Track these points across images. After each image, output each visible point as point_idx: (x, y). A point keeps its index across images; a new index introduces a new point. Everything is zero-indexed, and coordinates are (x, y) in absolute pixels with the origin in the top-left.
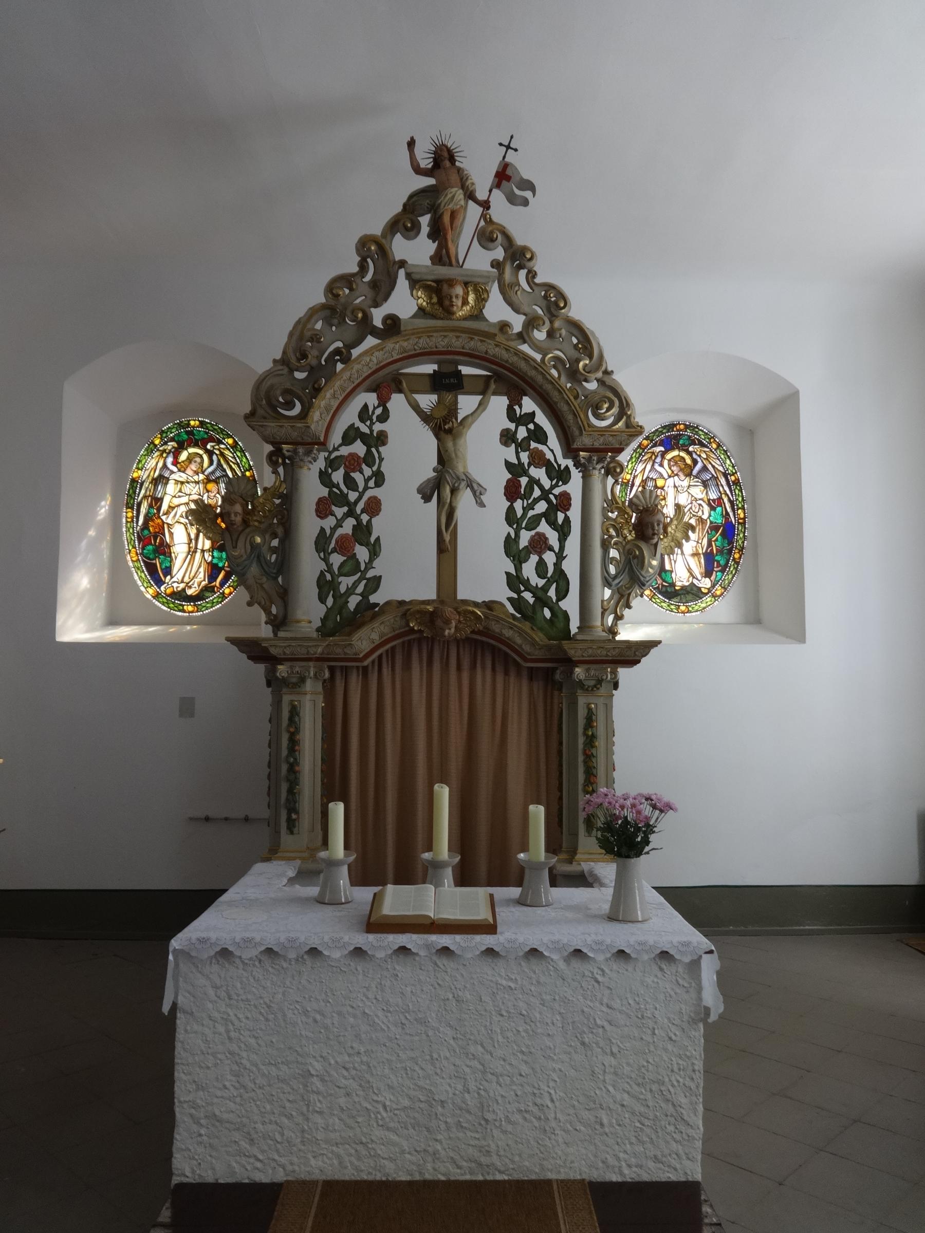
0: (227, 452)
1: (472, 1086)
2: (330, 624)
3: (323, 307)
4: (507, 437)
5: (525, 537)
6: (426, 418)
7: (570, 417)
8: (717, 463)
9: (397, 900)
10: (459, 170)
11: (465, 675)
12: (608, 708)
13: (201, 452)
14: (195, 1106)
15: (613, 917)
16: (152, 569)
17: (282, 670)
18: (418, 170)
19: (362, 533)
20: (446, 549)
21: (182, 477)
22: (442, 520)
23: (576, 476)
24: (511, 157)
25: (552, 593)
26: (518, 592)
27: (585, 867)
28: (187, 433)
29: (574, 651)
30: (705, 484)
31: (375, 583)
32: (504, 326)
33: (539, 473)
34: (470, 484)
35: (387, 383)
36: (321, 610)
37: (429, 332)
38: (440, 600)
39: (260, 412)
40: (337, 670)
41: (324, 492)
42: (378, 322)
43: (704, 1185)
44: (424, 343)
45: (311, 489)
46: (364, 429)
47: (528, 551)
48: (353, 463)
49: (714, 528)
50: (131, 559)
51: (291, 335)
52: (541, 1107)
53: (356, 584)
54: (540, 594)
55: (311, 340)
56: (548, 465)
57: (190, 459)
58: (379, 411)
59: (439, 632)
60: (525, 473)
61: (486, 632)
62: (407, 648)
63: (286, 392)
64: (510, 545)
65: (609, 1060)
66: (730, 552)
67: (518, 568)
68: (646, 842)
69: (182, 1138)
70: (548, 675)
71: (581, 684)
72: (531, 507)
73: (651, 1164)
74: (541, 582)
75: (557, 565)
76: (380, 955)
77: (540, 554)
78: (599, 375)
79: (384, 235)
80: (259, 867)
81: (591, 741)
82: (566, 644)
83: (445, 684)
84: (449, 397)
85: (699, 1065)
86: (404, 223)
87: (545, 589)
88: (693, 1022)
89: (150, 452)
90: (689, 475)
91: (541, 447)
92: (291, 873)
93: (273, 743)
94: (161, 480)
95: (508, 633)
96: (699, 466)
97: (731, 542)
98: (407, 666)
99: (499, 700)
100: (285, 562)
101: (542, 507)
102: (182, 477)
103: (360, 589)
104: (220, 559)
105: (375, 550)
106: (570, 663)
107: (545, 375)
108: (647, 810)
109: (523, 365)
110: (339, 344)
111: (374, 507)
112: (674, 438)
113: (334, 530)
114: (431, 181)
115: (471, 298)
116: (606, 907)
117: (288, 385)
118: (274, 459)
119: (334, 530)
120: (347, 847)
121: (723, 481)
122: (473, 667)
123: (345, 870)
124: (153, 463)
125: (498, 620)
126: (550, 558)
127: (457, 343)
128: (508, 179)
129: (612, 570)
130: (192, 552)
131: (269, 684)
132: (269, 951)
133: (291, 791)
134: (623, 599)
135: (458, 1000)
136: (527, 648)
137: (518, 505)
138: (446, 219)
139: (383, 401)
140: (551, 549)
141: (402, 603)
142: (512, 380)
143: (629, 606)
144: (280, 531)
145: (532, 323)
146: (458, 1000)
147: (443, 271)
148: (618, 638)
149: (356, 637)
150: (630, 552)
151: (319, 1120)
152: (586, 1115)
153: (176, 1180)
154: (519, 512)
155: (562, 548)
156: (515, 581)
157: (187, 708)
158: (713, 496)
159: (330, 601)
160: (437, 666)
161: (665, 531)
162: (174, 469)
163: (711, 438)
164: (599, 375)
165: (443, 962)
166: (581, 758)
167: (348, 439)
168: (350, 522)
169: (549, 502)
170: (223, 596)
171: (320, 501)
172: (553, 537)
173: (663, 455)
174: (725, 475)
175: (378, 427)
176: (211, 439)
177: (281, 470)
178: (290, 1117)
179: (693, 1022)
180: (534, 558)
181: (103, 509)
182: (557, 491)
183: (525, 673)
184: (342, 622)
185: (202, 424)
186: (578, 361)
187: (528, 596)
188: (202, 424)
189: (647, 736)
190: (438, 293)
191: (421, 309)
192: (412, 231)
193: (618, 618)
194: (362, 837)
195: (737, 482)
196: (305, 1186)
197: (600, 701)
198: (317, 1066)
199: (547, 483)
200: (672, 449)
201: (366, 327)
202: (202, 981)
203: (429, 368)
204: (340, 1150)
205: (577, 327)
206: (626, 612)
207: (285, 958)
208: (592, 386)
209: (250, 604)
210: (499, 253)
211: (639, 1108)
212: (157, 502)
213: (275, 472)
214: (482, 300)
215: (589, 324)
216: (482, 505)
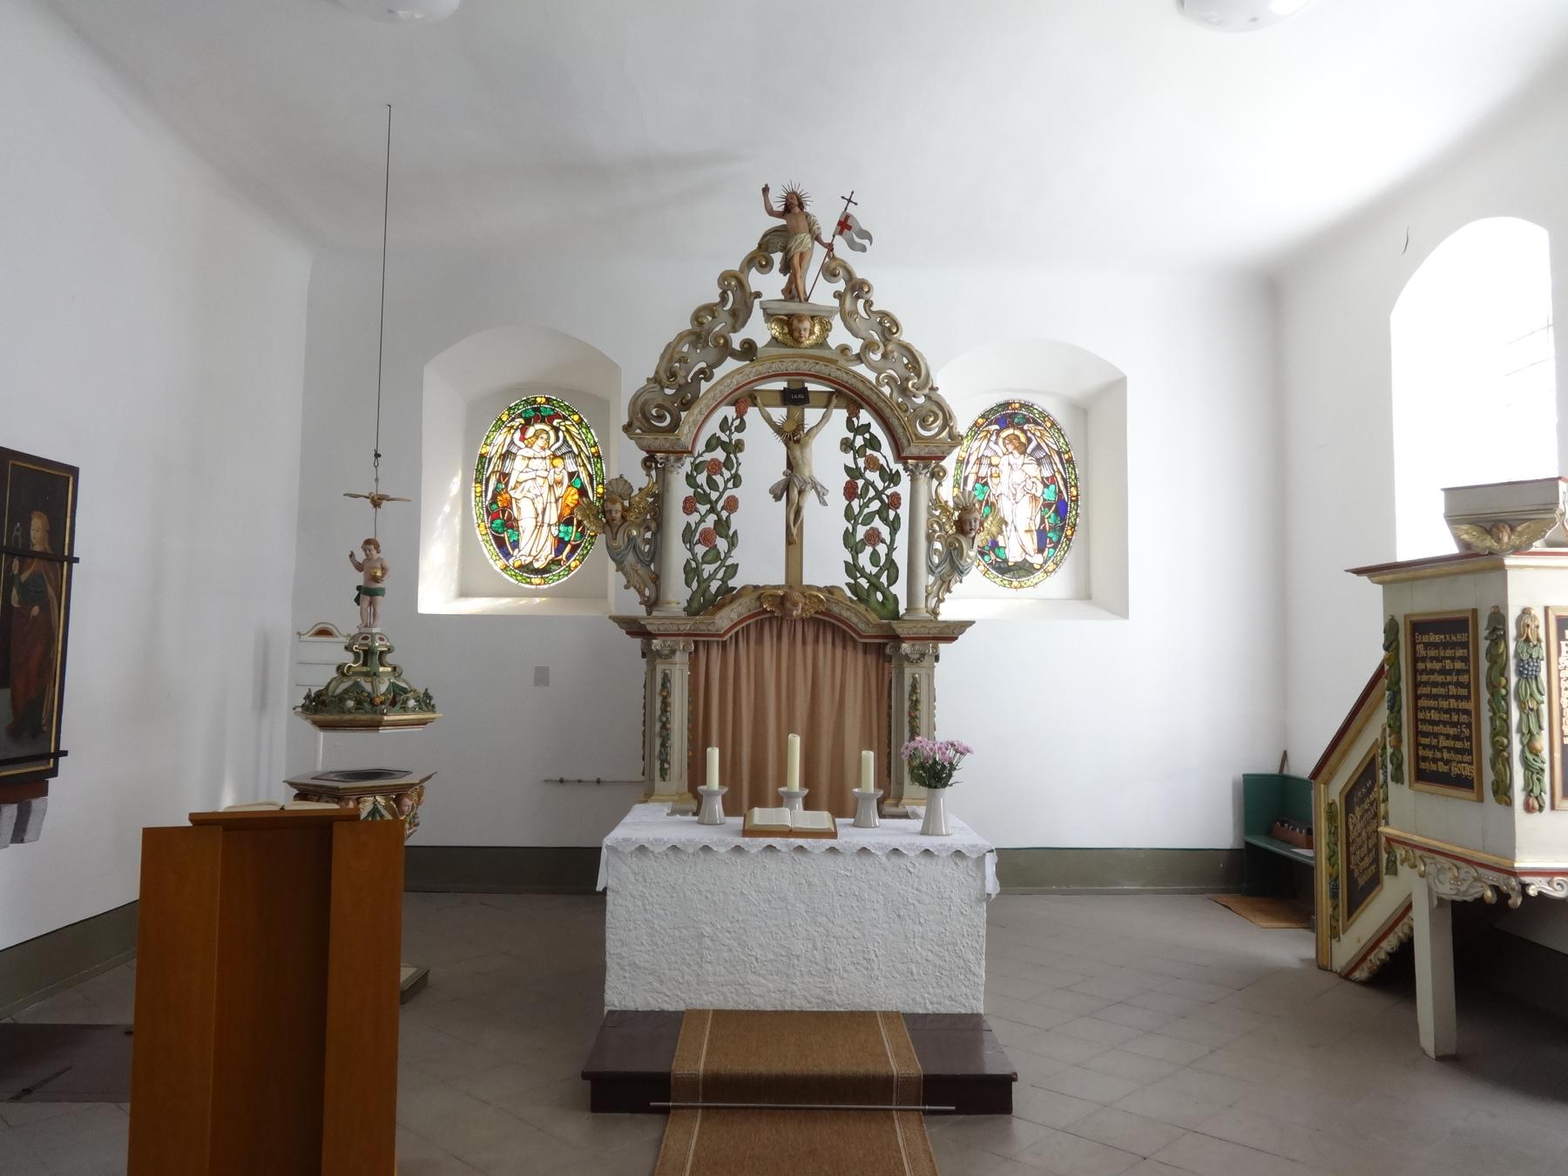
0: (572, 429)
1: (819, 945)
2: (695, 605)
3: (690, 333)
4: (847, 445)
5: (861, 532)
6: (779, 430)
7: (900, 430)
8: (1050, 441)
9: (760, 816)
10: (807, 215)
11: (809, 649)
12: (930, 677)
13: (547, 428)
14: (622, 958)
15: (923, 833)
16: (500, 543)
17: (656, 644)
18: (771, 213)
19: (722, 527)
20: (793, 541)
21: (528, 452)
22: (787, 518)
23: (905, 478)
24: (852, 209)
25: (884, 579)
26: (855, 579)
27: (909, 809)
28: (535, 410)
29: (901, 629)
30: (1039, 462)
31: (733, 569)
32: (844, 349)
33: (873, 476)
34: (815, 486)
35: (744, 398)
36: (688, 593)
37: (781, 358)
38: (789, 585)
39: (636, 423)
40: (701, 643)
41: (690, 492)
42: (736, 345)
43: (991, 1023)
44: (776, 367)
45: (680, 490)
46: (724, 438)
47: (864, 543)
48: (715, 467)
49: (1048, 505)
50: (481, 533)
51: (662, 357)
52: (868, 960)
53: (716, 572)
54: (874, 580)
55: (679, 361)
56: (881, 469)
57: (536, 435)
58: (737, 422)
59: (782, 612)
60: (861, 476)
61: (828, 613)
62: (760, 626)
63: (659, 406)
64: (848, 537)
65: (918, 928)
66: (1062, 529)
67: (855, 558)
68: (950, 776)
69: (611, 980)
70: (880, 649)
71: (907, 657)
72: (867, 505)
73: (947, 1002)
74: (875, 570)
75: (888, 555)
76: (753, 851)
77: (874, 546)
78: (926, 391)
79: (741, 270)
80: (637, 806)
81: (915, 704)
82: (895, 624)
83: (792, 657)
84: (796, 411)
85: (983, 932)
86: (759, 260)
87: (878, 576)
88: (979, 901)
89: (498, 428)
90: (1023, 453)
91: (875, 454)
92: (668, 810)
93: (647, 706)
94: (507, 455)
95: (846, 614)
96: (1034, 444)
97: (1063, 519)
98: (760, 641)
99: (838, 672)
100: (656, 553)
101: (875, 505)
102: (528, 452)
103: (720, 575)
104: (566, 533)
105: (733, 542)
106: (898, 639)
107: (879, 394)
108: (951, 753)
109: (860, 386)
110: (703, 365)
111: (732, 505)
112: (1007, 417)
113: (698, 524)
114: (782, 222)
115: (817, 329)
116: (920, 829)
117: (660, 401)
118: (648, 463)
119: (698, 524)
120: (722, 782)
121: (1056, 459)
122: (816, 641)
123: (719, 799)
124: (501, 439)
125: (838, 603)
126: (882, 549)
127: (804, 368)
128: (849, 228)
129: (936, 560)
130: (539, 526)
131: (644, 655)
132: (674, 847)
133: (663, 745)
134: (945, 584)
135: (810, 884)
136: (862, 626)
137: (856, 504)
138: (796, 261)
139: (741, 414)
140: (883, 541)
141: (756, 588)
142: (851, 397)
143: (949, 591)
144: (653, 525)
145: (869, 346)
146: (810, 884)
147: (793, 307)
148: (940, 618)
149: (718, 616)
150: (951, 545)
151: (708, 967)
152: (901, 966)
153: (606, 1009)
154: (856, 510)
155: (892, 541)
156: (852, 569)
157: (542, 676)
158: (1047, 473)
159: (695, 585)
160: (785, 640)
161: (982, 524)
162: (521, 445)
163: (1045, 415)
164: (926, 391)
165: (798, 857)
166: (907, 719)
167: (710, 447)
168: (712, 518)
169: (882, 501)
170: (569, 569)
171: (687, 500)
172: (885, 531)
173: (998, 433)
174: (1059, 453)
175: (736, 436)
176: (557, 416)
177: (653, 473)
178: (689, 966)
179: (979, 901)
180: (869, 550)
181: (455, 485)
182: (888, 492)
183: (860, 648)
184: (705, 603)
185: (548, 400)
186: (908, 380)
187: (863, 582)
188: (548, 400)
189: (961, 697)
190: (789, 325)
191: (774, 338)
192: (766, 266)
193: (940, 601)
194: (729, 774)
195: (1070, 461)
196: (701, 1013)
197: (923, 672)
198: (708, 930)
199: (880, 485)
200: (1007, 427)
201: (726, 350)
202: (625, 869)
203: (781, 385)
204: (725, 989)
205: (907, 349)
206: (947, 596)
207: (685, 852)
208: (920, 400)
209: (626, 587)
210: (841, 286)
211: (938, 962)
212: (505, 476)
213: (648, 475)
214: (826, 328)
215: (918, 346)
216: (824, 503)
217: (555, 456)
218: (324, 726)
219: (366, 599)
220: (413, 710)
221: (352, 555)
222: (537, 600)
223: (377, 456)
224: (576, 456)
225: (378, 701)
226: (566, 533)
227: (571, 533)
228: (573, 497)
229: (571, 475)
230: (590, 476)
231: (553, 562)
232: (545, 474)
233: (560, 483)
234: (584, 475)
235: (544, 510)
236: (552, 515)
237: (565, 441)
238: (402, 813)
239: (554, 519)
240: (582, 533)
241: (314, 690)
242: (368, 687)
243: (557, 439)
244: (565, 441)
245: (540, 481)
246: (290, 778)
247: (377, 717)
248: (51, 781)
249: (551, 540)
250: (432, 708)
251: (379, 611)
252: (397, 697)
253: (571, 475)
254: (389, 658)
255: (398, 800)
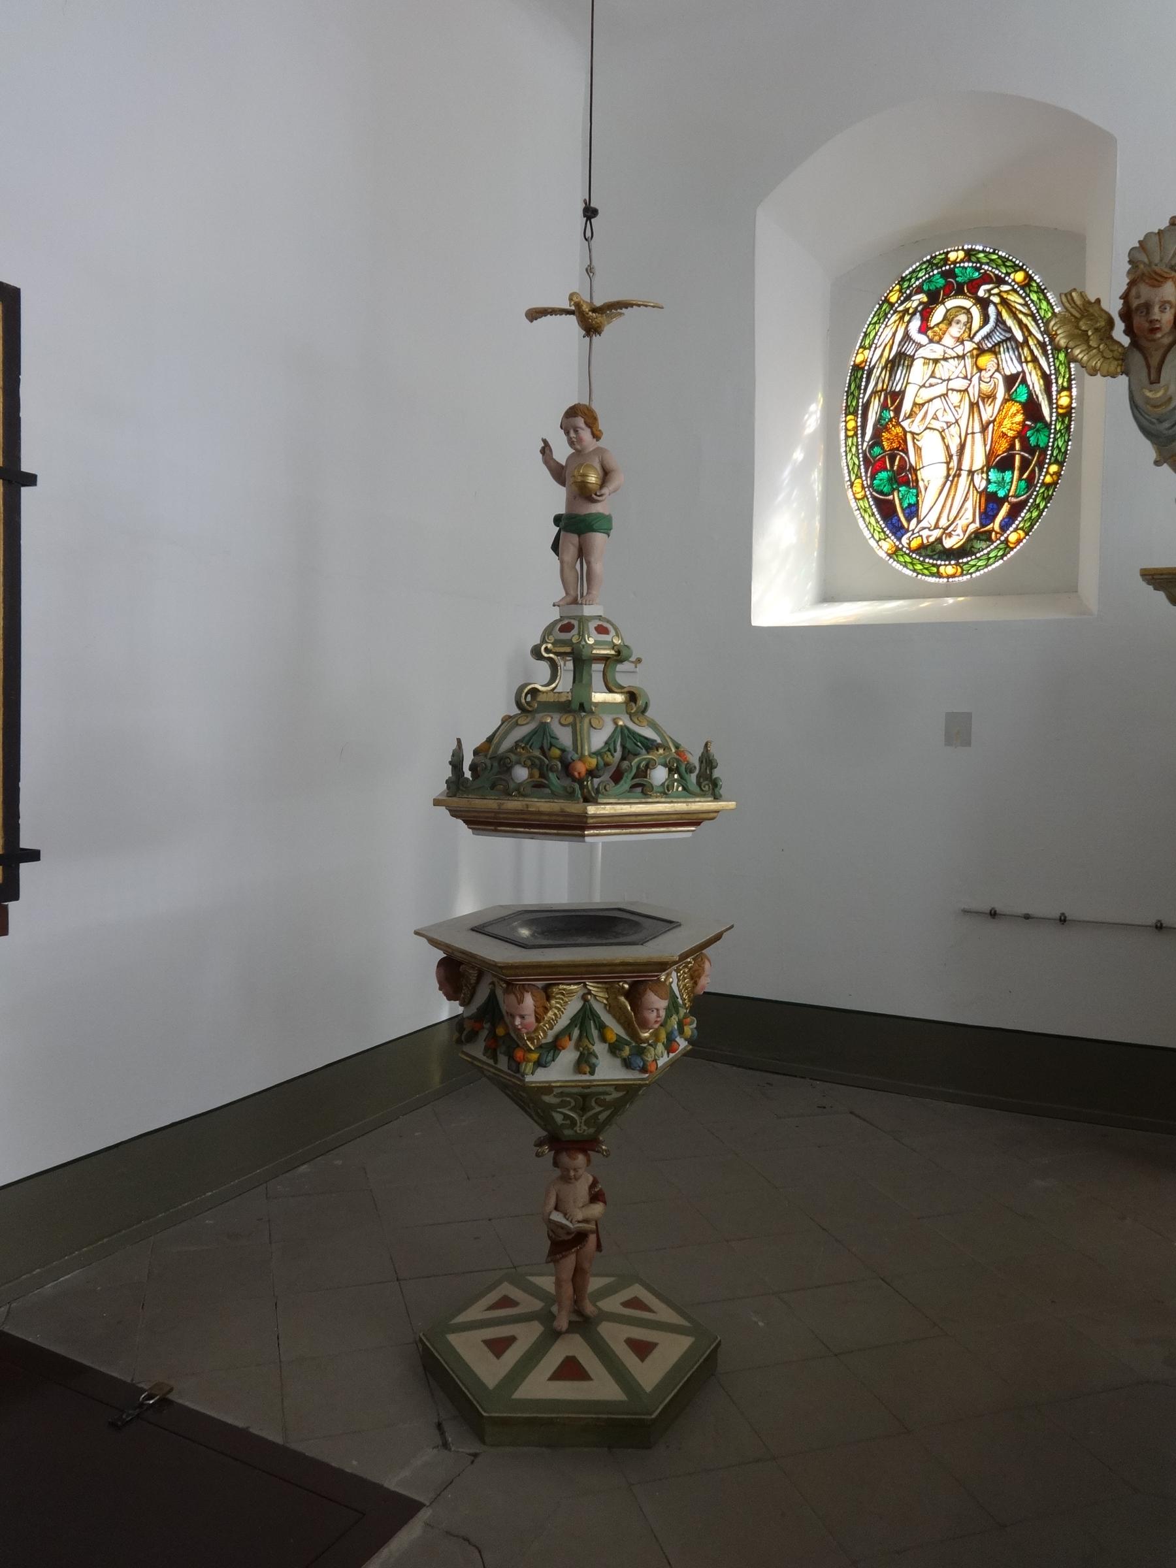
0: (1013, 298)
13: (967, 303)
16: (886, 510)
21: (936, 351)
28: (944, 275)
57: (948, 320)
89: (882, 317)
94: (900, 361)
102: (936, 351)
104: (1001, 483)
124: (888, 334)
130: (952, 477)
157: (958, 730)
162: (922, 339)
170: (1007, 546)
176: (986, 279)
181: (813, 418)
188: (969, 254)
212: (896, 397)
217: (981, 351)
218: (479, 822)
219: (571, 542)
220: (665, 791)
221: (546, 449)
222: (950, 601)
223: (590, 213)
224: (1019, 346)
225: (581, 768)
227: (1011, 483)
228: (1014, 419)
229: (1010, 381)
230: (1046, 378)
231: (977, 536)
232: (962, 384)
233: (990, 397)
234: (1035, 381)
235: (962, 447)
236: (977, 455)
237: (1000, 321)
238: (644, 1025)
239: (980, 461)
240: (1030, 482)
241: (472, 741)
242: (564, 736)
243: (986, 319)
244: (1000, 321)
245: (954, 398)
246: (418, 927)
247: (573, 807)
248: (12, 906)
249: (973, 497)
250: (709, 785)
251: (598, 567)
252: (629, 763)
253: (1010, 381)
254: (624, 674)
255: (635, 995)
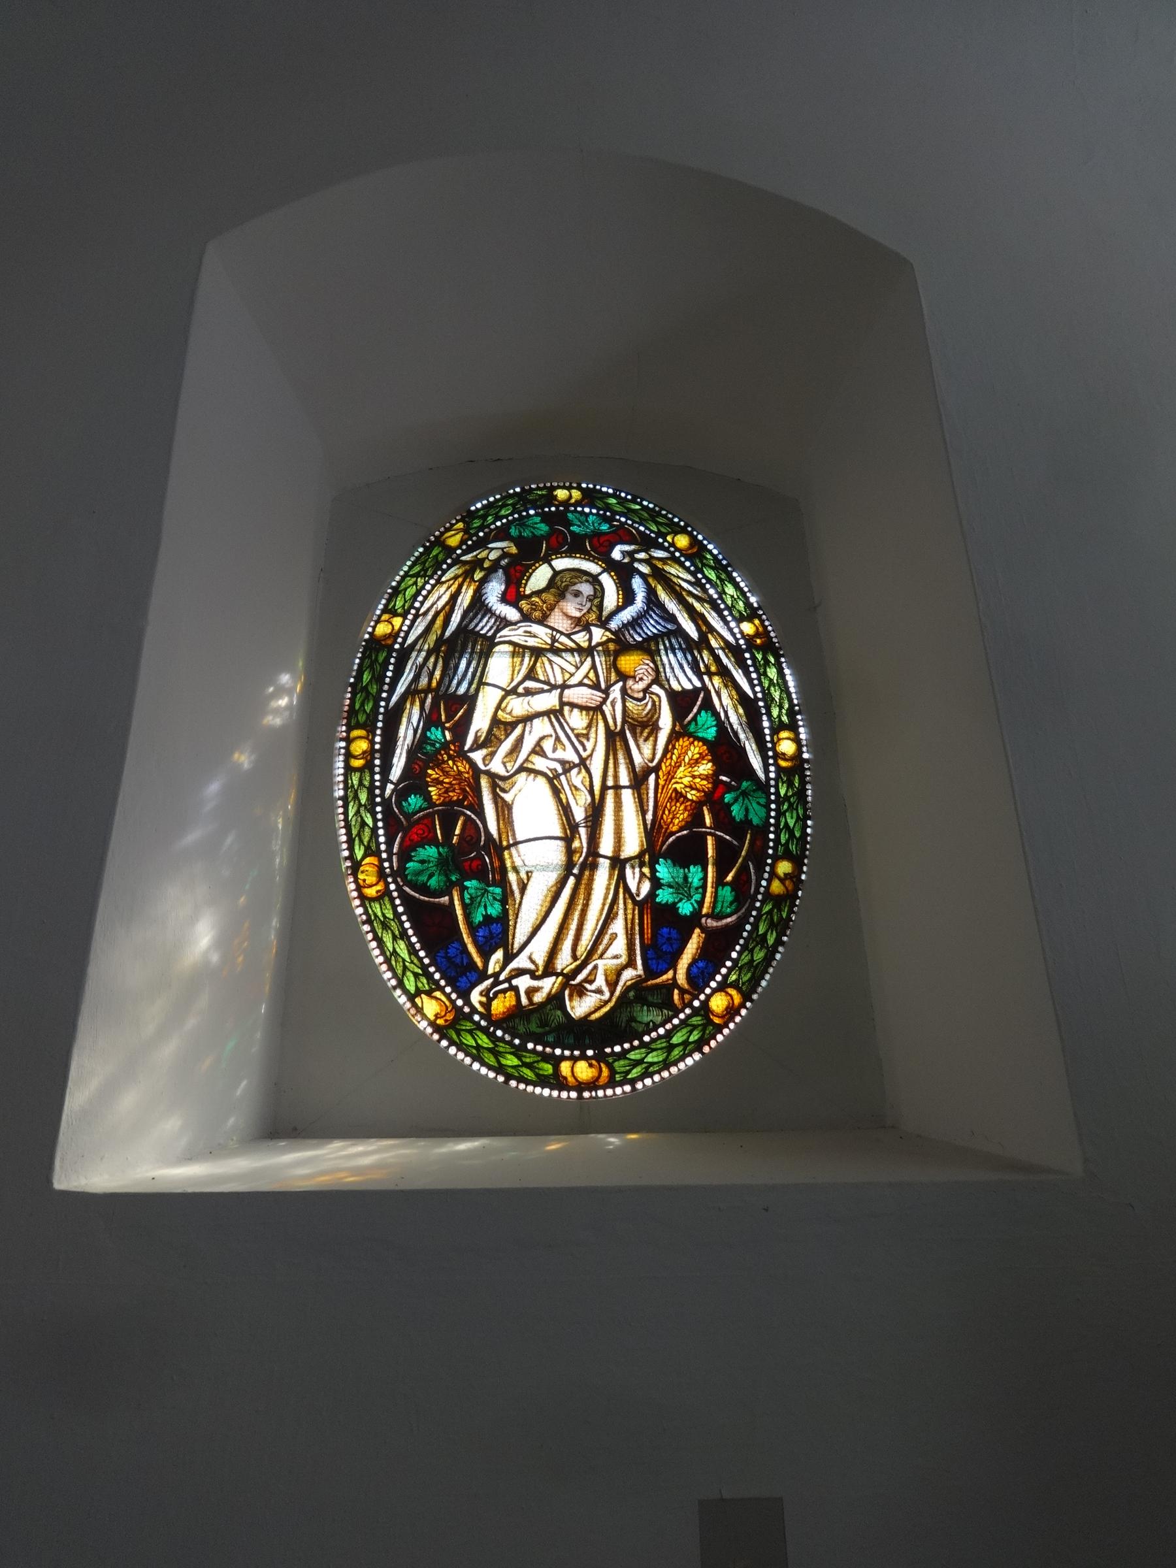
16: (433, 927)
57: (559, 587)
94: (467, 642)
130: (578, 868)
162: (512, 614)
170: (708, 1024)
181: (283, 698)
188: (590, 497)
217: (620, 645)
224: (691, 647)
226: (682, 888)
228: (694, 772)
229: (682, 702)
231: (638, 994)
233: (646, 726)
234: (725, 701)
237: (651, 593)
239: (633, 844)
243: (628, 597)
245: (577, 720)
253: (682, 702)
